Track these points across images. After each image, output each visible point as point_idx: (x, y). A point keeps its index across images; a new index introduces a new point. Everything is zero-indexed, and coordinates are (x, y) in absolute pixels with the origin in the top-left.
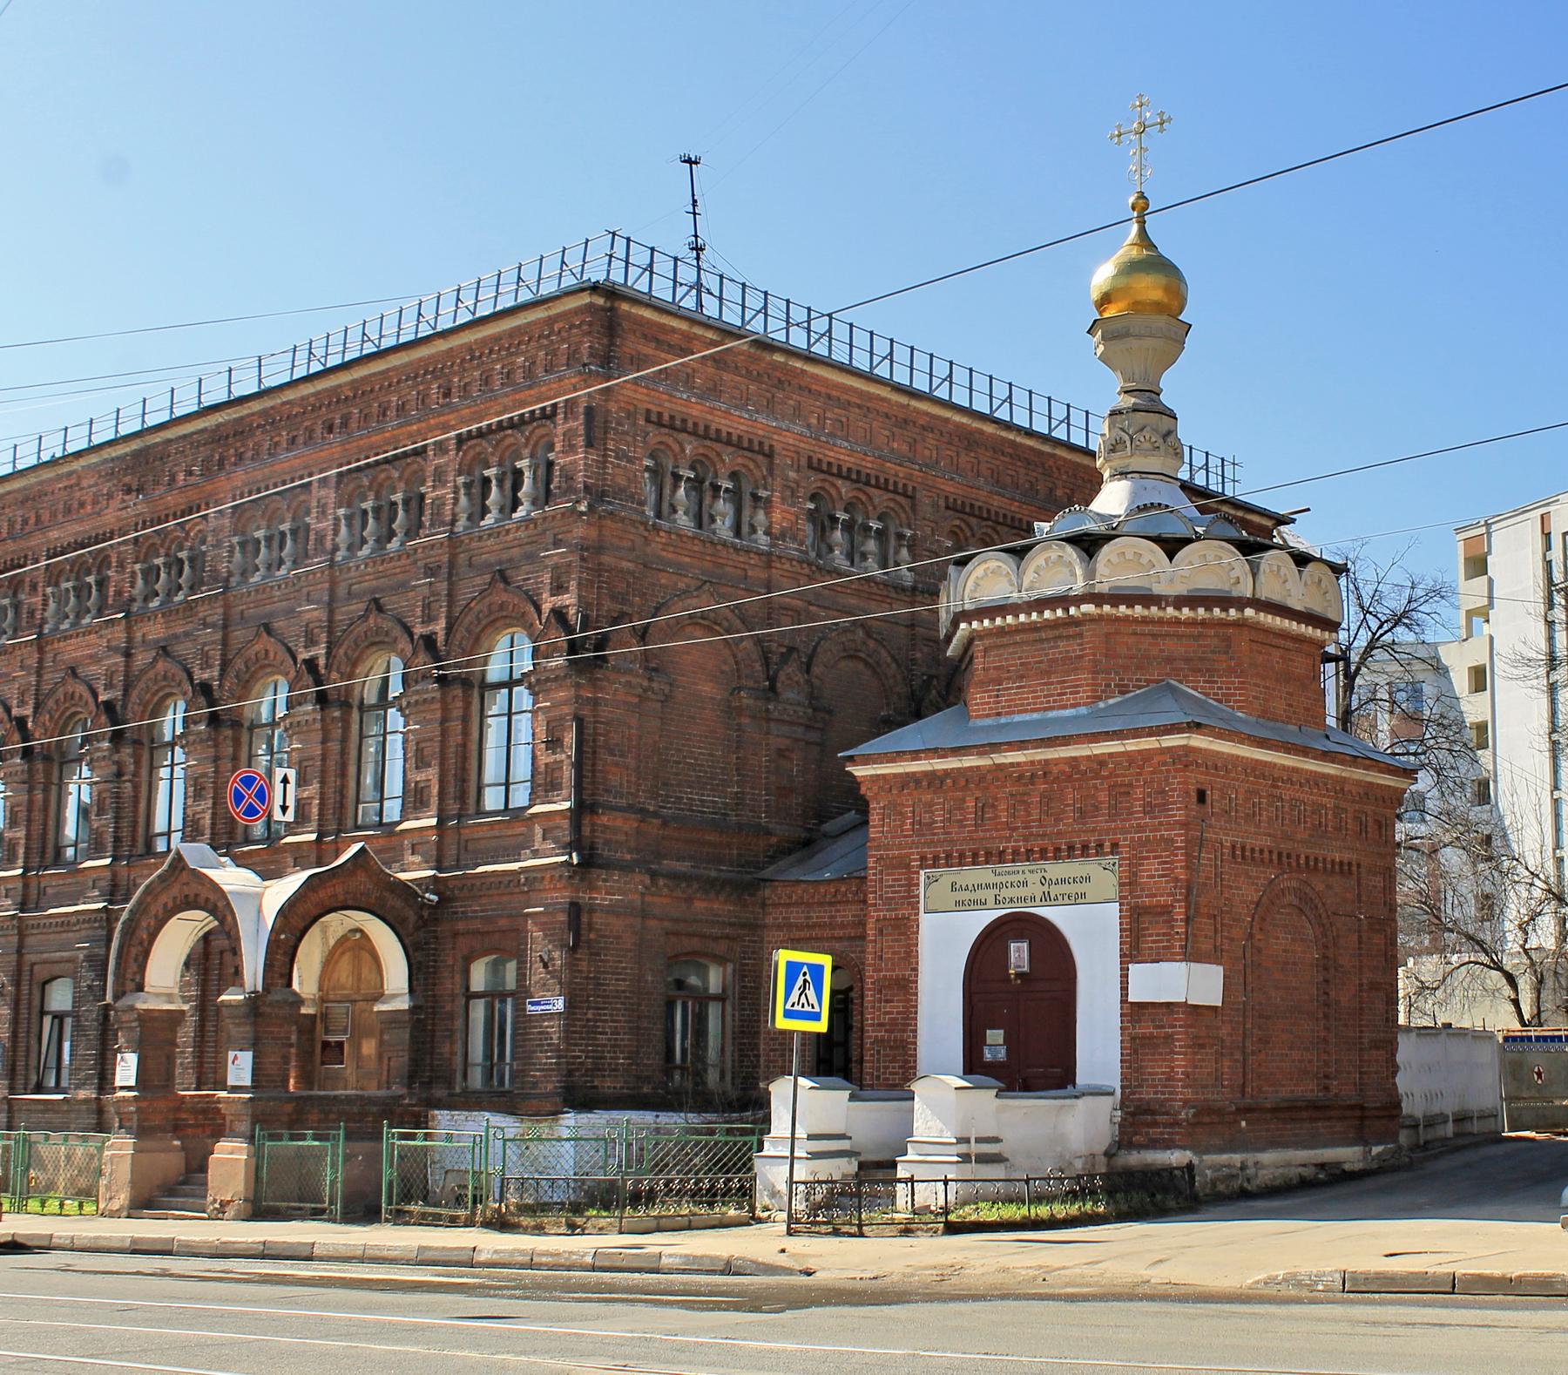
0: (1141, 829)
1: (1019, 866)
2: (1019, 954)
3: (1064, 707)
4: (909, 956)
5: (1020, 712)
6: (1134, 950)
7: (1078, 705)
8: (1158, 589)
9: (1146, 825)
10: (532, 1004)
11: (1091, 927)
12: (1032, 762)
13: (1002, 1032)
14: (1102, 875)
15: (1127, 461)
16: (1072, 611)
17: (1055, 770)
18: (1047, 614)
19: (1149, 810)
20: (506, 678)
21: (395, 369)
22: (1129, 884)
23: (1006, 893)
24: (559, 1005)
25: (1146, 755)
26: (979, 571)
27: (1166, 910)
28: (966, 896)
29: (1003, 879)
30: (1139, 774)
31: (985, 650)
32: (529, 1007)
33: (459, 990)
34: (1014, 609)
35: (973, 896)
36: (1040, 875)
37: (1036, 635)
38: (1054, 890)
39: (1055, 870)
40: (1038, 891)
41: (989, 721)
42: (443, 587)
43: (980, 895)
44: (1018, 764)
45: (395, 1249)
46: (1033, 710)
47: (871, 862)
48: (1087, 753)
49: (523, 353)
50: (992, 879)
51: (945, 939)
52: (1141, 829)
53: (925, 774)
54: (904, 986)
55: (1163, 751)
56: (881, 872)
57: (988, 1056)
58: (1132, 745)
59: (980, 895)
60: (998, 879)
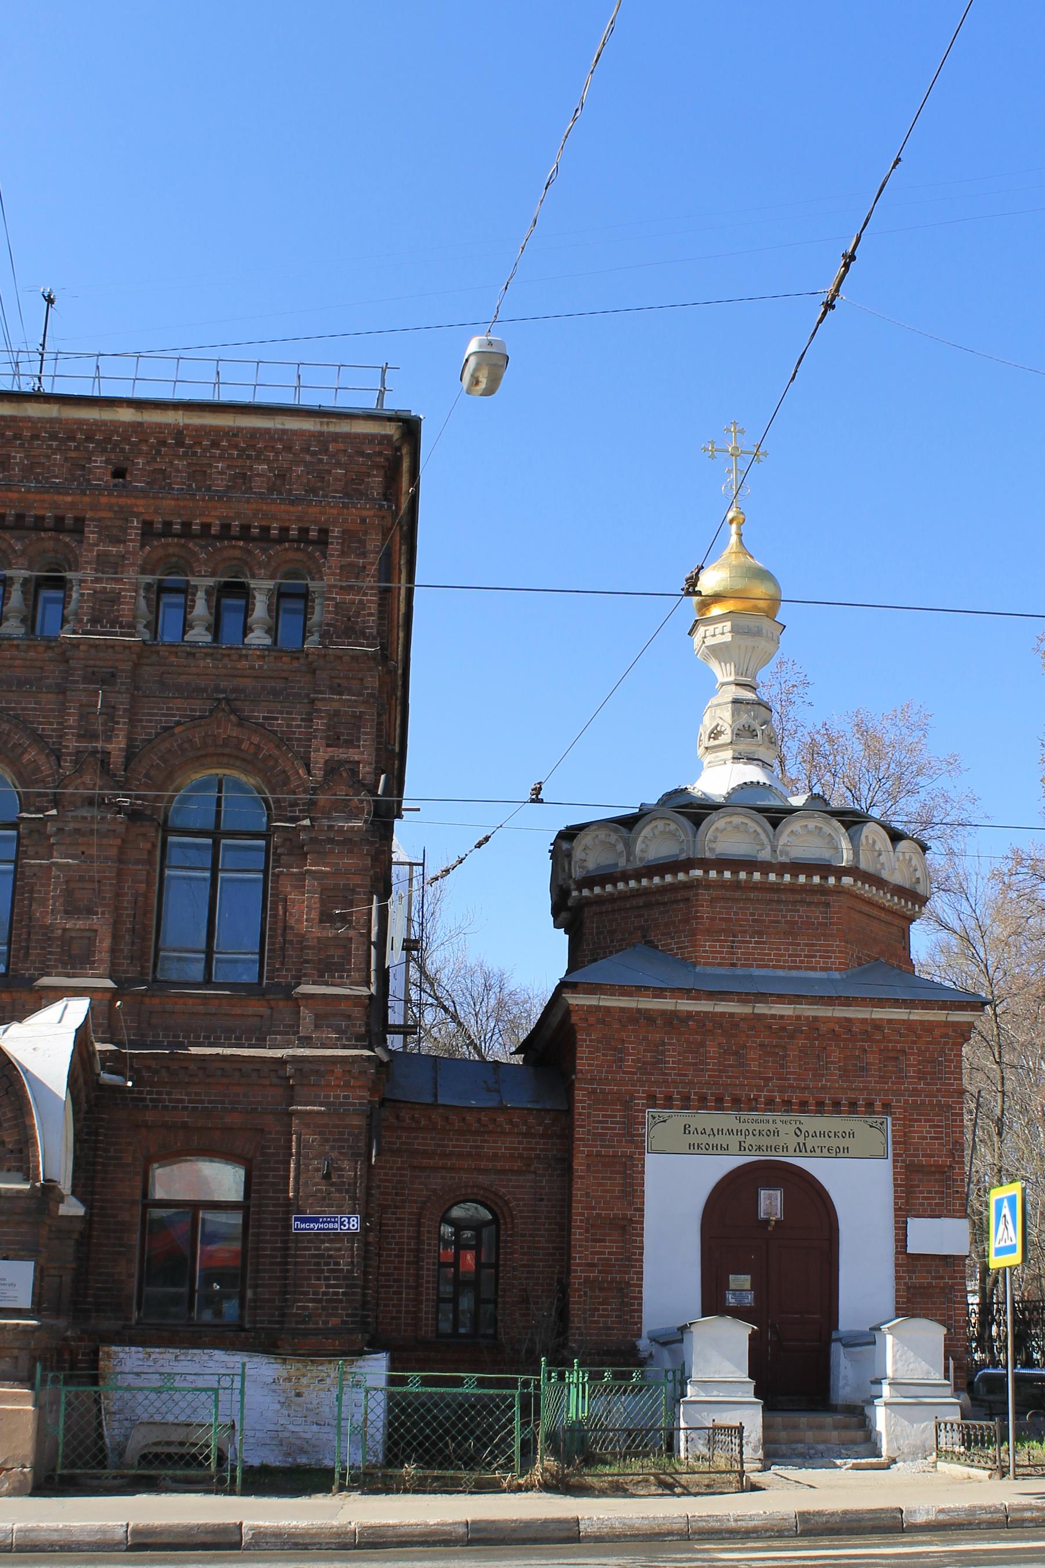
0: (915, 1092)
1: (769, 1116)
2: (771, 1203)
3: (814, 969)
5: (759, 966)
6: (907, 1206)
7: (831, 969)
8: (885, 875)
9: (923, 1090)
10: (304, 1220)
12: (798, 1018)
13: (748, 1277)
14: (875, 1133)
15: (754, 748)
16: (832, 880)
17: (823, 1028)
18: (597, 890)
19: (921, 1076)
20: (210, 825)
21: (29, 419)
22: (902, 1142)
23: (750, 1140)
24: (353, 1224)
25: (928, 1027)
28: (704, 1139)
29: (751, 1127)
30: (914, 1042)
31: (712, 900)
32: (295, 1224)
33: (138, 1196)
34: (765, 867)
35: (711, 1140)
38: (810, 1142)
39: (812, 1123)
40: (792, 1141)
42: (122, 701)
43: (719, 1140)
44: (782, 1017)
45: (751, 1518)
48: (860, 1016)
49: (266, 460)
50: (735, 1125)
51: (677, 1183)
52: (915, 1092)
53: (663, 1012)
54: (627, 1227)
55: (947, 1024)
58: (918, 1015)
59: (719, 1140)
60: (744, 1127)
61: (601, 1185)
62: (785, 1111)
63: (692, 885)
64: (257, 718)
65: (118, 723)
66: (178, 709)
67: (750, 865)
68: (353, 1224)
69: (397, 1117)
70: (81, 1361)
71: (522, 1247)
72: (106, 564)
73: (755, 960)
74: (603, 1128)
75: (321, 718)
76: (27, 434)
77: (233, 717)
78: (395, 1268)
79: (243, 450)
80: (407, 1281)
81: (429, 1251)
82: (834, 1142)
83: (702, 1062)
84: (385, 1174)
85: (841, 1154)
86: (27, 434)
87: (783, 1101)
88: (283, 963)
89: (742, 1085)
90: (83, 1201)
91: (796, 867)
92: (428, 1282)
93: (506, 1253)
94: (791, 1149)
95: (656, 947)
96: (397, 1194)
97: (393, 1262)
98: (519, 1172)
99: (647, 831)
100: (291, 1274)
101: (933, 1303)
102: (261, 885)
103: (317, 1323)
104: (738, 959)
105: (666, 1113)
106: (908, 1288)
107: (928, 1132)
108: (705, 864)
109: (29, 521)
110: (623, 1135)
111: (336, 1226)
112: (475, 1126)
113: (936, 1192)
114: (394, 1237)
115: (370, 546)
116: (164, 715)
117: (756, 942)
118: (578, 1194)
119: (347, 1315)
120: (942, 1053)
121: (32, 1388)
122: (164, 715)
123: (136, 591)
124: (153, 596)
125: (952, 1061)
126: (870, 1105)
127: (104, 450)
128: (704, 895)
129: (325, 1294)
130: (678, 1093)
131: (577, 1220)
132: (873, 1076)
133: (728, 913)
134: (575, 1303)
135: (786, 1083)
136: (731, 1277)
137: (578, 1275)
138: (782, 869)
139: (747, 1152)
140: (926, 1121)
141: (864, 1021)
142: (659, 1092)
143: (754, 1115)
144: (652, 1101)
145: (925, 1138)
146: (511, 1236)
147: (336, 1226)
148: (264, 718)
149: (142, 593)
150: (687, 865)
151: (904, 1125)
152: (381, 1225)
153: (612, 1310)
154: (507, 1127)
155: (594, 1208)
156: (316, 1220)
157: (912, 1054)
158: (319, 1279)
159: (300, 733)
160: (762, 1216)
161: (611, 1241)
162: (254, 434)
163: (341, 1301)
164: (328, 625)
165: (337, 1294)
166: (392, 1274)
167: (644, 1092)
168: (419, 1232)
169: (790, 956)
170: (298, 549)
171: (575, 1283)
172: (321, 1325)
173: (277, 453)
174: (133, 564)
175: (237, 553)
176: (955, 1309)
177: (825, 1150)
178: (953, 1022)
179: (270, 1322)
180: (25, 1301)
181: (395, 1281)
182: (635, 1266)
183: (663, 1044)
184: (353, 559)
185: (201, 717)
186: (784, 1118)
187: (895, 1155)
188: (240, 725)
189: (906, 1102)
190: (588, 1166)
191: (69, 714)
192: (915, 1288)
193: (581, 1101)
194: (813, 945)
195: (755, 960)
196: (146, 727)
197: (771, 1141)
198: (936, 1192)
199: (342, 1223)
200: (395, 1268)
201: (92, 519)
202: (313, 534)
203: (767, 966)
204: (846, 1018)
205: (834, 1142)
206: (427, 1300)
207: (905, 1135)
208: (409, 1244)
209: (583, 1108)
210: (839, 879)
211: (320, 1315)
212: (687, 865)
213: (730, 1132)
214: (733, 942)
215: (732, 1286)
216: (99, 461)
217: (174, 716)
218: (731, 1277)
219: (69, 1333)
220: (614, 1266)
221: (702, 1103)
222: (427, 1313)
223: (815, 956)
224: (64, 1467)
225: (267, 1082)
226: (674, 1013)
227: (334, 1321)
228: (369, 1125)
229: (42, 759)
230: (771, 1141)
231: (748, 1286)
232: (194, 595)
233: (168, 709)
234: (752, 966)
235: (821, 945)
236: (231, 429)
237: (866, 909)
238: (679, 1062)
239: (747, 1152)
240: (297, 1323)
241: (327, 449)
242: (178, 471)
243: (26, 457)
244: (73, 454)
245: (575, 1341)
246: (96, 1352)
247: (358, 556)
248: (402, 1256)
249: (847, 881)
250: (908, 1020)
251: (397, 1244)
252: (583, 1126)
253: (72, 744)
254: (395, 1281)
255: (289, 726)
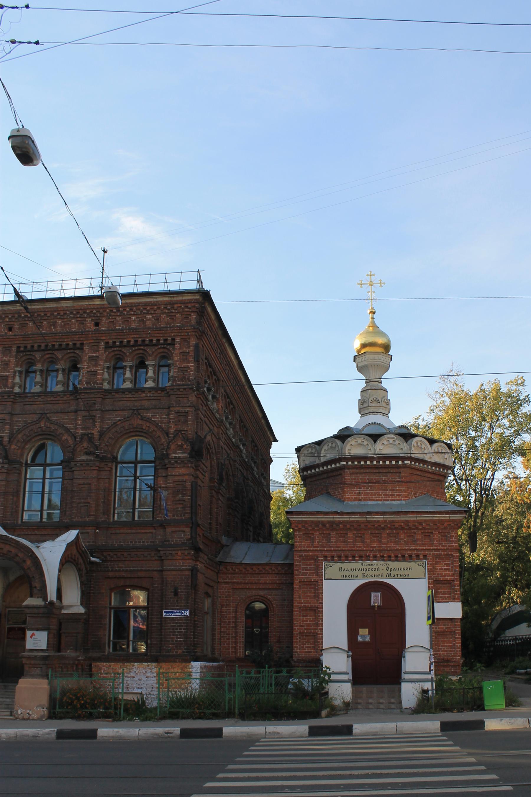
1: (375, 562)
2: (376, 599)
3: (394, 500)
4: (318, 595)
5: (371, 500)
7: (401, 500)
10: (167, 612)
11: (413, 589)
12: (386, 521)
13: (367, 630)
14: (419, 568)
18: (309, 472)
20: (133, 459)
23: (367, 573)
24: (186, 613)
26: (353, 443)
27: (449, 583)
28: (347, 573)
29: (367, 567)
32: (164, 614)
33: (108, 606)
34: (318, 466)
36: (386, 566)
37: (377, 471)
38: (393, 573)
40: (385, 573)
41: (356, 503)
43: (354, 573)
44: (379, 521)
46: (377, 500)
47: (296, 557)
49: (151, 314)
51: (336, 592)
52: (437, 550)
53: (329, 522)
54: (316, 610)
55: (450, 521)
56: (300, 562)
57: (360, 639)
58: (437, 517)
60: (364, 567)
61: (306, 593)
62: (382, 560)
63: (343, 468)
64: (149, 416)
65: (96, 422)
66: (119, 415)
67: (365, 458)
68: (186, 613)
69: (226, 569)
70: (86, 669)
71: (277, 620)
72: (94, 360)
73: (369, 498)
74: (306, 570)
75: (172, 414)
76: (62, 313)
77: (139, 416)
78: (227, 629)
79: (142, 311)
80: (232, 634)
81: (240, 622)
82: (403, 572)
83: (347, 542)
84: (223, 592)
85: (406, 577)
86: (62, 313)
87: (381, 556)
88: (160, 512)
89: (363, 550)
90: (85, 607)
91: (385, 458)
92: (240, 634)
93: (271, 622)
94: (385, 577)
95: (331, 495)
96: (227, 600)
97: (226, 627)
98: (275, 589)
99: (326, 447)
100: (163, 634)
101: (447, 638)
102: (41, 484)
103: (173, 652)
104: (362, 498)
105: (332, 563)
106: (435, 632)
107: (443, 566)
108: (347, 459)
109: (64, 346)
110: (315, 573)
111: (180, 614)
112: (257, 571)
113: (447, 592)
114: (226, 617)
115: (191, 344)
116: (114, 417)
117: (369, 490)
118: (296, 598)
119: (185, 649)
120: (449, 533)
121: (48, 679)
122: (114, 417)
123: (103, 370)
124: (112, 371)
125: (453, 536)
126: (418, 556)
127: (90, 317)
128: (347, 472)
129: (176, 641)
130: (336, 555)
131: (295, 608)
132: (419, 544)
133: (358, 479)
134: (295, 642)
135: (382, 548)
136: (360, 630)
137: (297, 631)
138: (379, 459)
139: (366, 578)
140: (442, 562)
141: (414, 521)
142: (328, 554)
143: (368, 563)
144: (326, 558)
145: (442, 569)
146: (273, 615)
147: (180, 614)
148: (152, 416)
149: (106, 370)
150: (339, 460)
151: (433, 564)
152: (221, 612)
153: (311, 644)
154: (270, 571)
155: (303, 603)
156: (172, 612)
157: (436, 534)
158: (174, 635)
159: (165, 421)
160: (372, 604)
161: (310, 616)
162: (145, 304)
163: (182, 644)
164: (175, 377)
165: (181, 641)
166: (226, 632)
167: (322, 555)
168: (236, 614)
169: (384, 495)
170: (164, 348)
171: (295, 633)
172: (175, 653)
173: (155, 310)
174: (101, 360)
175: (141, 351)
176: (456, 641)
177: (399, 576)
178: (453, 520)
179: (156, 652)
180: (44, 647)
181: (227, 634)
182: (319, 626)
183: (330, 534)
184: (184, 350)
185: (128, 417)
186: (382, 563)
187: (429, 577)
188: (142, 419)
189: (433, 554)
190: (300, 586)
191: (79, 420)
192: (439, 632)
193: (297, 560)
194: (393, 490)
195: (369, 498)
196: (108, 423)
197: (376, 573)
198: (447, 592)
199: (182, 613)
200: (227, 629)
201: (87, 344)
202: (169, 341)
203: (374, 500)
204: (406, 520)
205: (403, 572)
206: (240, 642)
207: (433, 568)
208: (232, 619)
209: (297, 562)
210: (403, 462)
211: (174, 649)
212: (339, 460)
213: (359, 570)
214: (360, 491)
215: (360, 633)
216: (89, 321)
217: (118, 417)
218: (360, 630)
219: (80, 658)
220: (311, 626)
221: (347, 558)
222: (240, 647)
223: (394, 495)
224: (59, 708)
225: (153, 559)
226: (333, 522)
227: (180, 652)
228: (192, 574)
229: (69, 438)
230: (376, 573)
231: (367, 633)
232: (126, 369)
233: (116, 415)
234: (368, 500)
235: (397, 490)
236: (137, 303)
237: (418, 473)
238: (337, 542)
239: (366, 578)
240: (166, 652)
241: (174, 307)
242: (118, 321)
243: (62, 322)
244: (79, 319)
245: (296, 657)
246: (91, 665)
247: (186, 348)
248: (230, 624)
249: (407, 462)
250: (433, 520)
251: (227, 619)
252: (298, 570)
253: (80, 432)
254: (227, 634)
255: (161, 418)
